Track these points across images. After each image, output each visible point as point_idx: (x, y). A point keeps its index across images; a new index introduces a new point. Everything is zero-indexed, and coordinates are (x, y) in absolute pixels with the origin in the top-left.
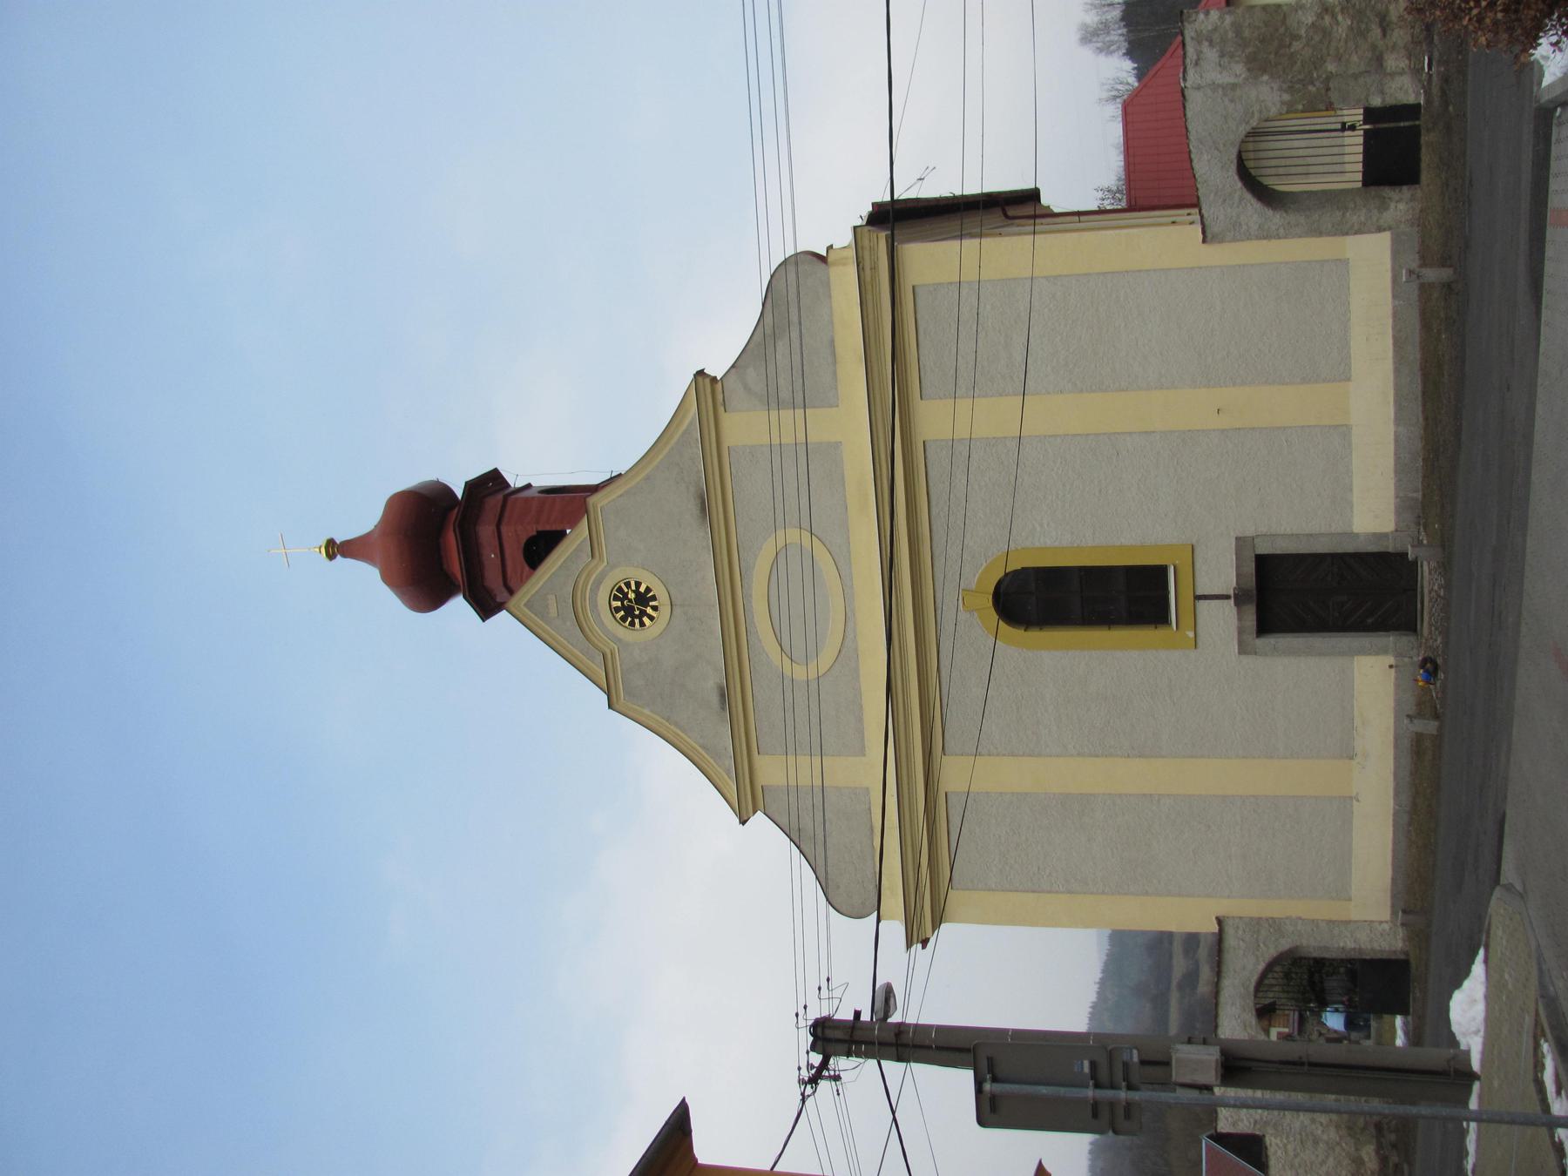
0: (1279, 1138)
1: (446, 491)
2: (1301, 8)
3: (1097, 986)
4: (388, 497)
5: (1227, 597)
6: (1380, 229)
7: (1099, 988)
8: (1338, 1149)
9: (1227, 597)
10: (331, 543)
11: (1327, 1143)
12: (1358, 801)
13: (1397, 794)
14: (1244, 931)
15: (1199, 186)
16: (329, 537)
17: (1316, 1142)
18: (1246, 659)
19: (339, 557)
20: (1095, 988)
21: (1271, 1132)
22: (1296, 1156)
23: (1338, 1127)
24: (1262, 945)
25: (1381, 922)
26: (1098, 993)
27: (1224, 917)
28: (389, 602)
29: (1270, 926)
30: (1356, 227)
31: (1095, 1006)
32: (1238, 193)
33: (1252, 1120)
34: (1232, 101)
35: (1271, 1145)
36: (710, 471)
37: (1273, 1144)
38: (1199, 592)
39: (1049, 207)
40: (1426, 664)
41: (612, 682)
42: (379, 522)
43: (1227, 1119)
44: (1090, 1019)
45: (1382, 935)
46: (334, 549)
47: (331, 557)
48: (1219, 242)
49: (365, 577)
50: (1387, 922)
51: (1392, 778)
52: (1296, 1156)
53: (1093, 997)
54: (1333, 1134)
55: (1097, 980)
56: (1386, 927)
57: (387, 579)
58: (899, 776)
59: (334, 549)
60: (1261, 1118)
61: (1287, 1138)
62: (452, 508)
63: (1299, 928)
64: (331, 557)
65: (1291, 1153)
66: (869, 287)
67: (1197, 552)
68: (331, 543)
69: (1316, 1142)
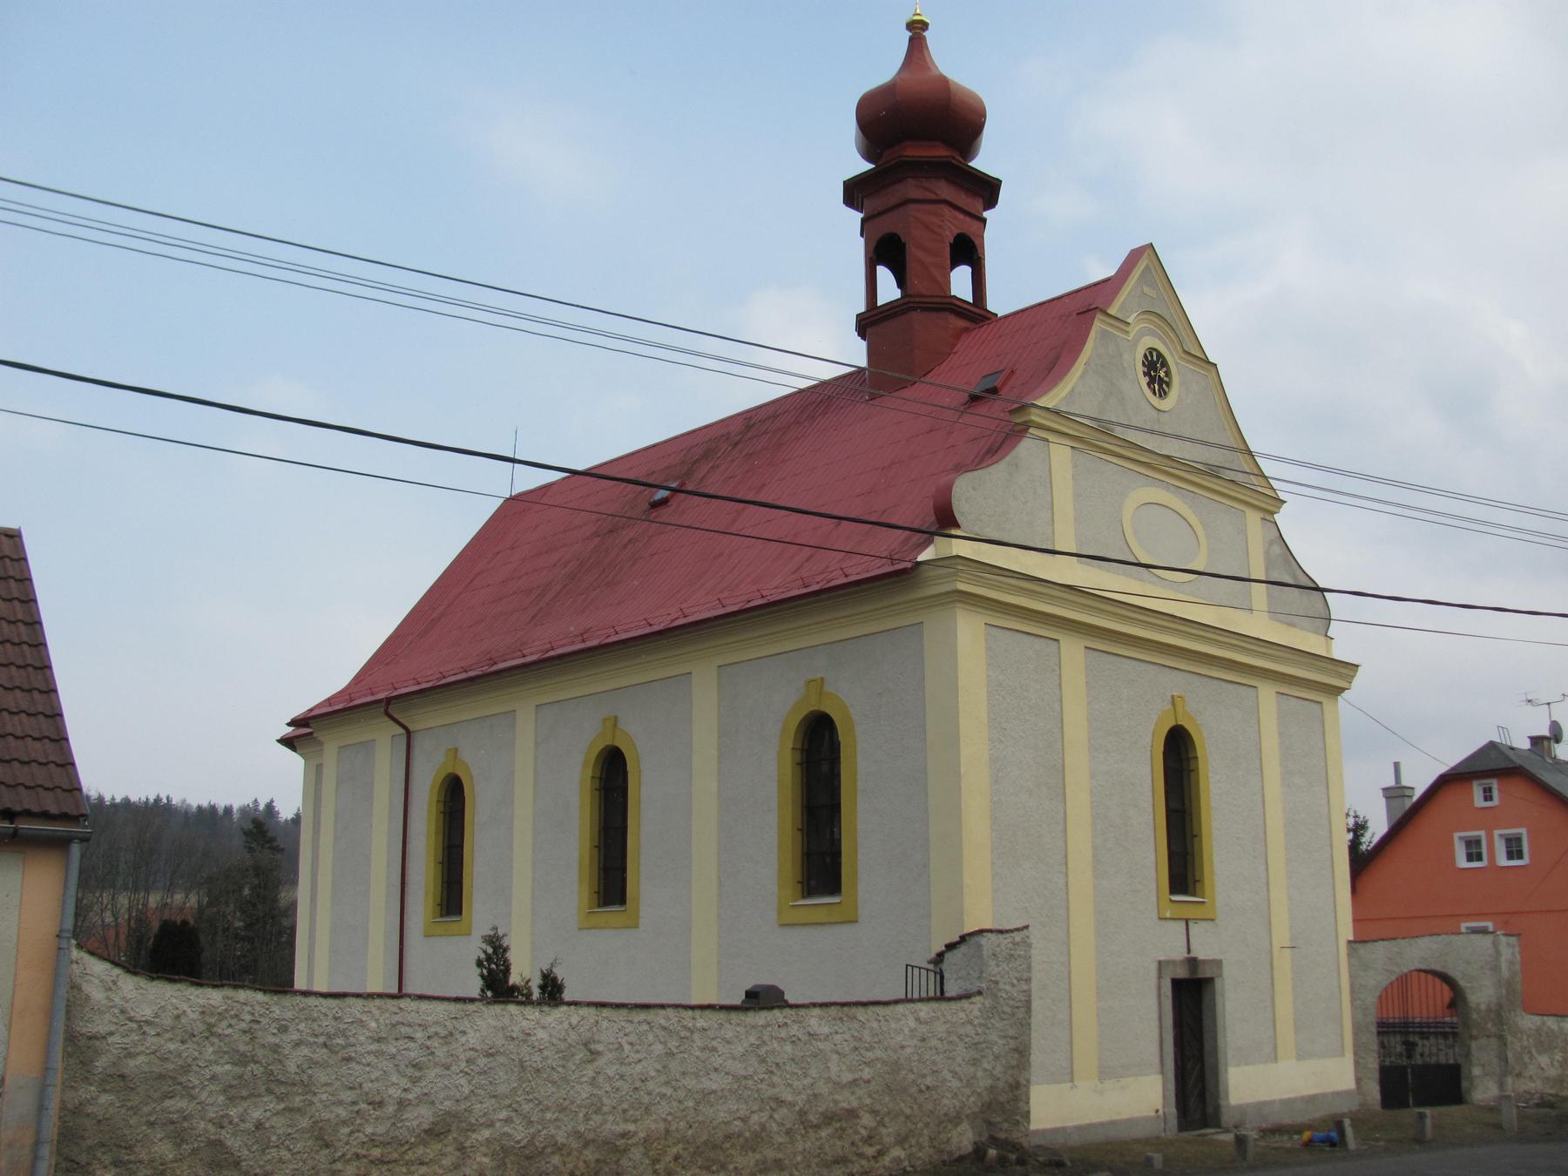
0: (979, 1014)
5: (1189, 951)
6: (1358, 1080)
8: (967, 1091)
9: (1189, 951)
10: (924, 26)
11: (974, 1077)
12: (1072, 1088)
13: (1078, 1128)
15: (1407, 940)
17: (975, 1062)
18: (1154, 967)
21: (986, 1002)
22: (960, 1037)
23: (992, 1089)
30: (1361, 1061)
32: (1395, 969)
33: (998, 978)
34: (1482, 968)
35: (972, 1003)
36: (1254, 496)
37: (972, 1006)
38: (1191, 924)
40: (997, 1147)
41: (1112, 321)
43: (999, 946)
46: (917, 29)
48: (1348, 954)
51: (1088, 1122)
52: (960, 1037)
54: (984, 1083)
58: (1104, 600)
59: (917, 29)
60: (1000, 990)
61: (980, 1025)
65: (962, 1031)
66: (1313, 661)
67: (1210, 923)
68: (924, 26)
69: (975, 1062)
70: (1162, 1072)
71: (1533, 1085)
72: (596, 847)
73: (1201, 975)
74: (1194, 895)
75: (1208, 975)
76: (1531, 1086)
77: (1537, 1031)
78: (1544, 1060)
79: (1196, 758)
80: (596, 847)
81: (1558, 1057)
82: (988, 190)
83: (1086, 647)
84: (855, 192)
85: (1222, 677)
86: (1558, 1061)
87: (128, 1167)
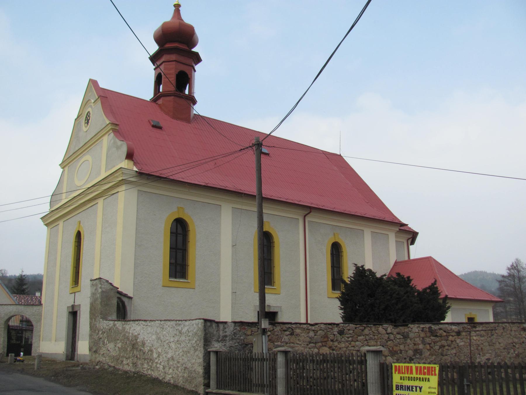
1: (194, 45)
2: (134, 363)
3: (492, 272)
4: (194, 26)
7: (492, 273)
14: (38, 312)
16: (181, 5)
19: (174, 8)
20: (492, 272)
24: (34, 317)
25: (39, 350)
26: (490, 273)
27: (43, 306)
28: (156, 25)
29: (39, 319)
31: (485, 273)
39: (156, 125)
42: (185, 22)
44: (481, 272)
45: (36, 350)
46: (177, 7)
47: (175, 6)
49: (167, 16)
50: (39, 351)
53: (488, 272)
55: (494, 273)
56: (38, 351)
57: (165, 24)
59: (177, 7)
62: (188, 47)
63: (38, 327)
64: (175, 6)
70: (77, 354)
71: (104, 359)
72: (74, 281)
73: (75, 310)
74: (187, 280)
75: (76, 310)
76: (102, 359)
77: (110, 330)
78: (111, 346)
79: (343, 252)
80: (74, 281)
81: (119, 345)
82: (197, 59)
83: (232, 207)
84: (154, 59)
85: (272, 213)
86: (118, 348)
87: (368, 341)
